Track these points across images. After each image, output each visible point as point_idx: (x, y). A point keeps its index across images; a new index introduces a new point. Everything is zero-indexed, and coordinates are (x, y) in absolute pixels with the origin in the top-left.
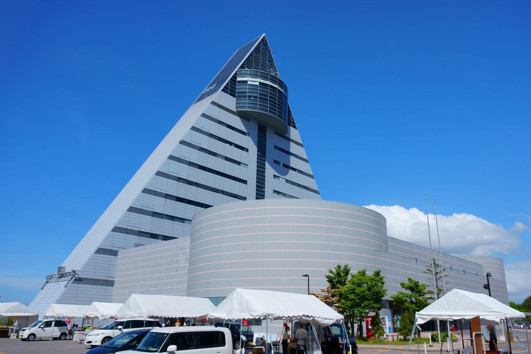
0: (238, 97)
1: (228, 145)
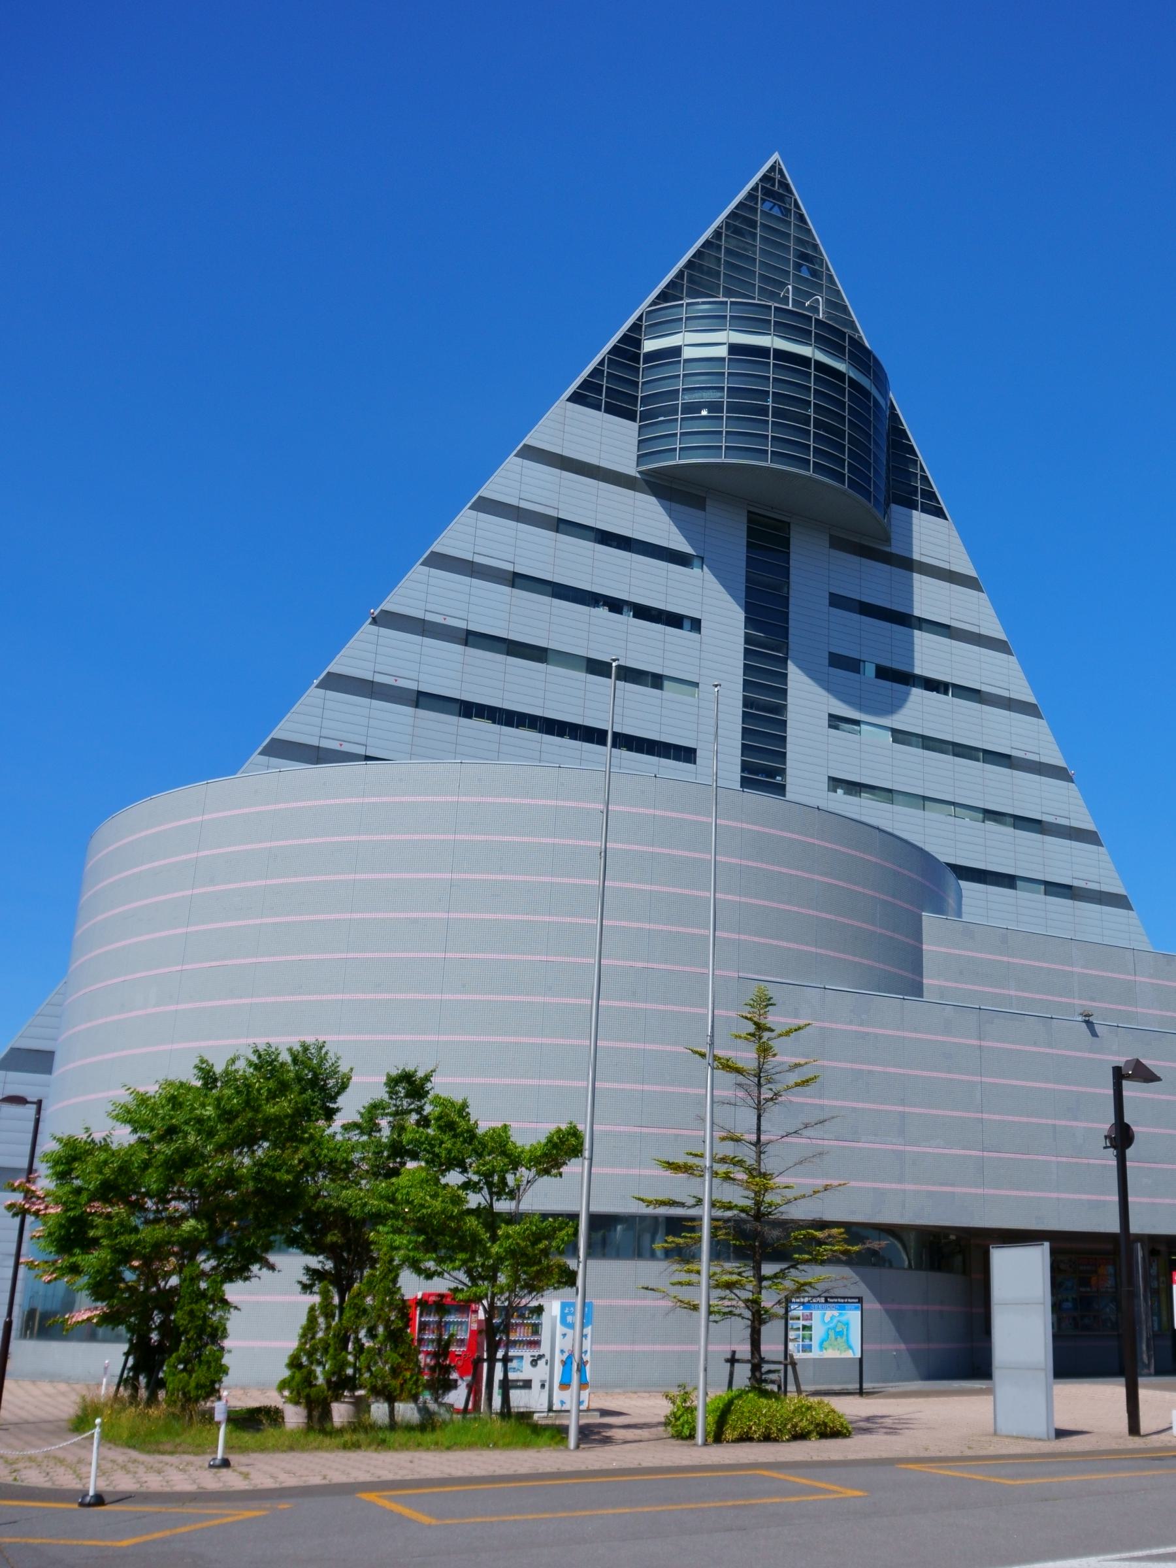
0: (645, 416)
1: (603, 612)
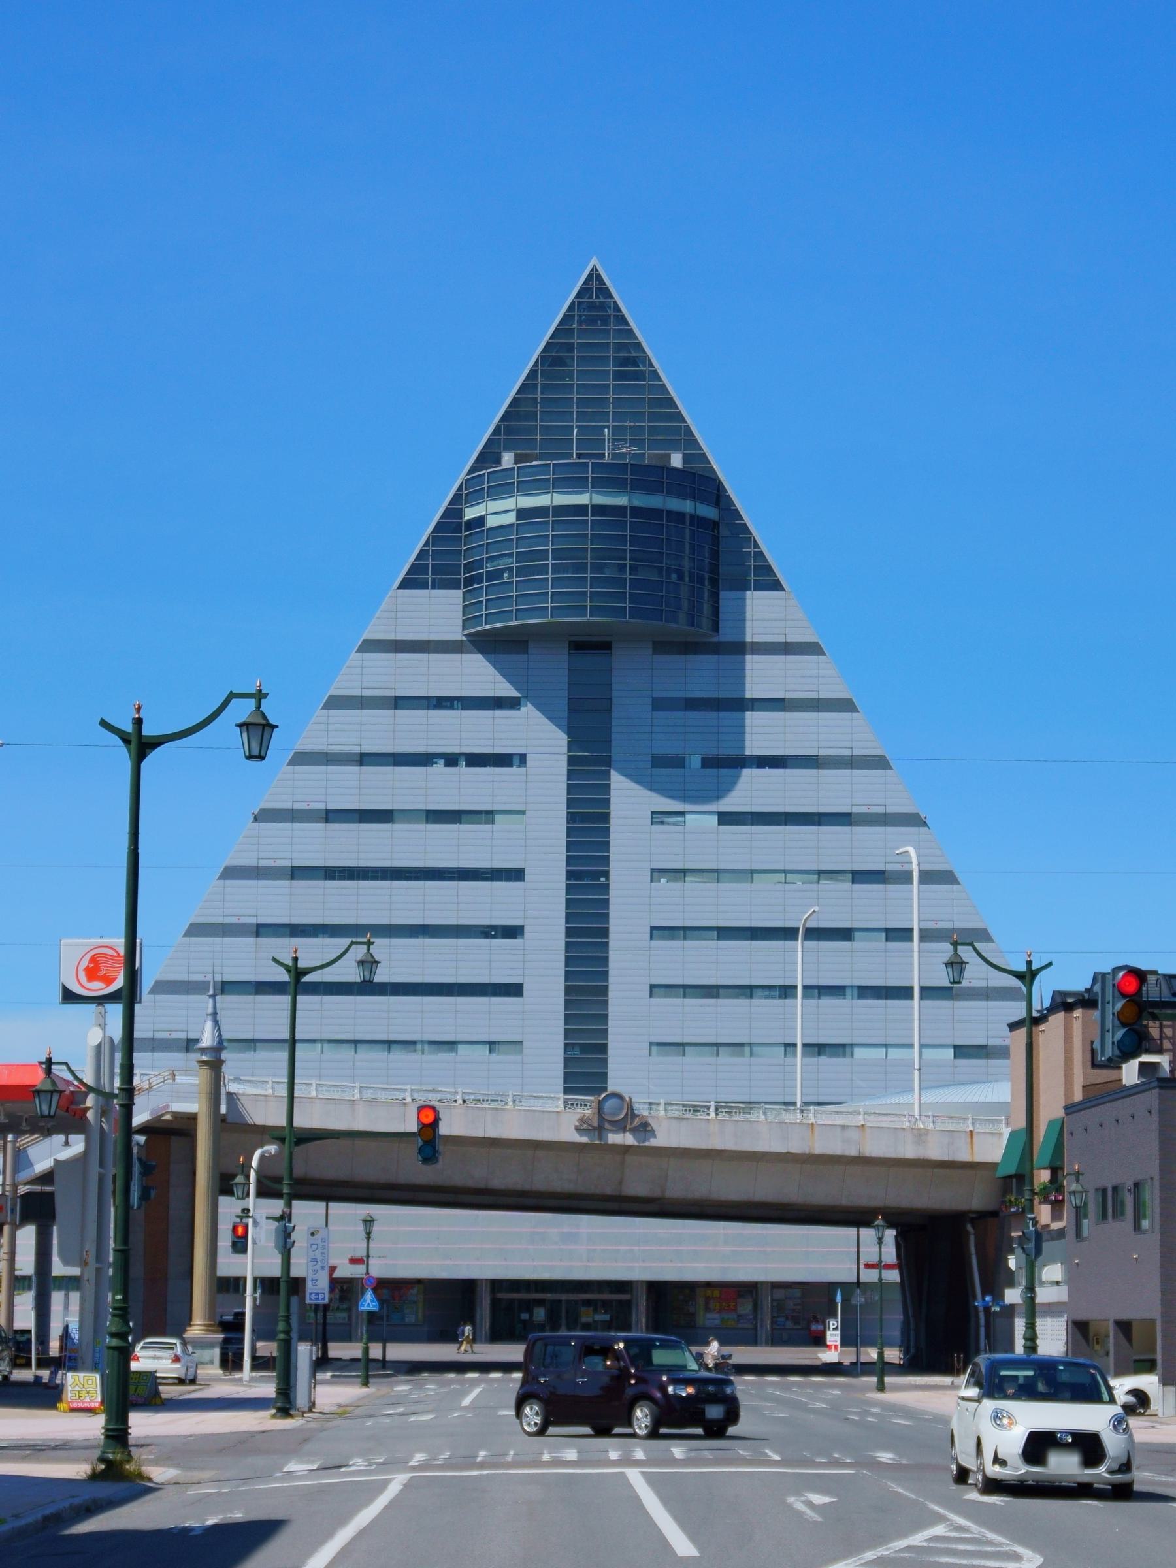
1: (439, 767)
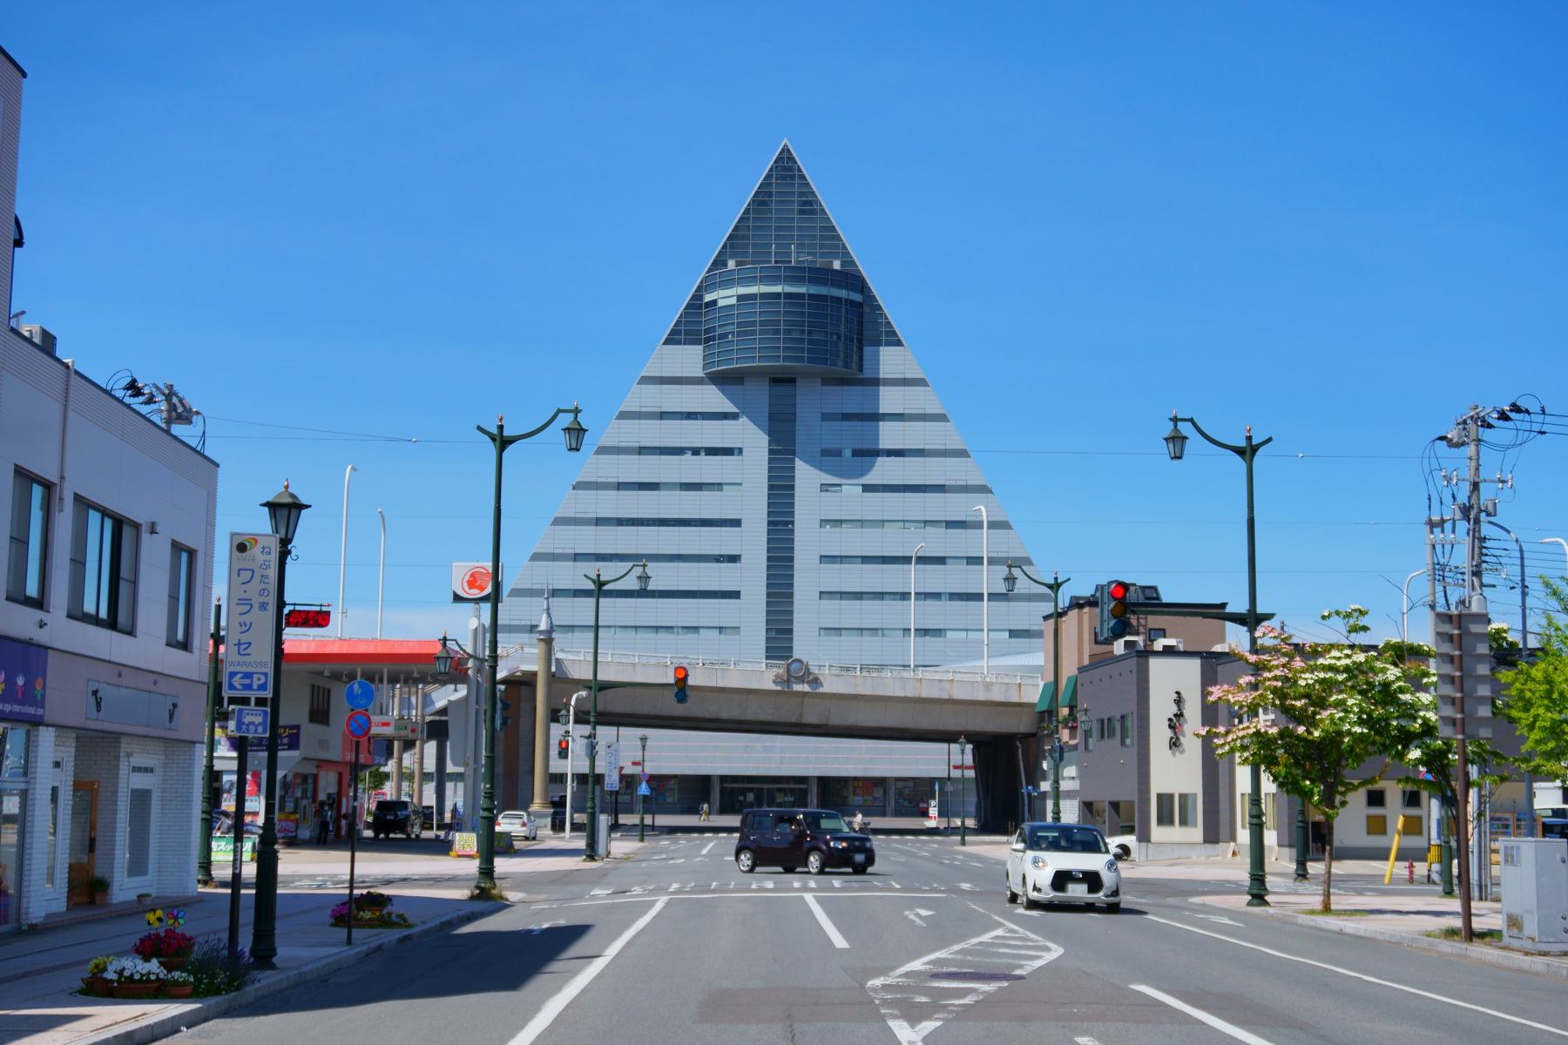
1: (688, 456)
